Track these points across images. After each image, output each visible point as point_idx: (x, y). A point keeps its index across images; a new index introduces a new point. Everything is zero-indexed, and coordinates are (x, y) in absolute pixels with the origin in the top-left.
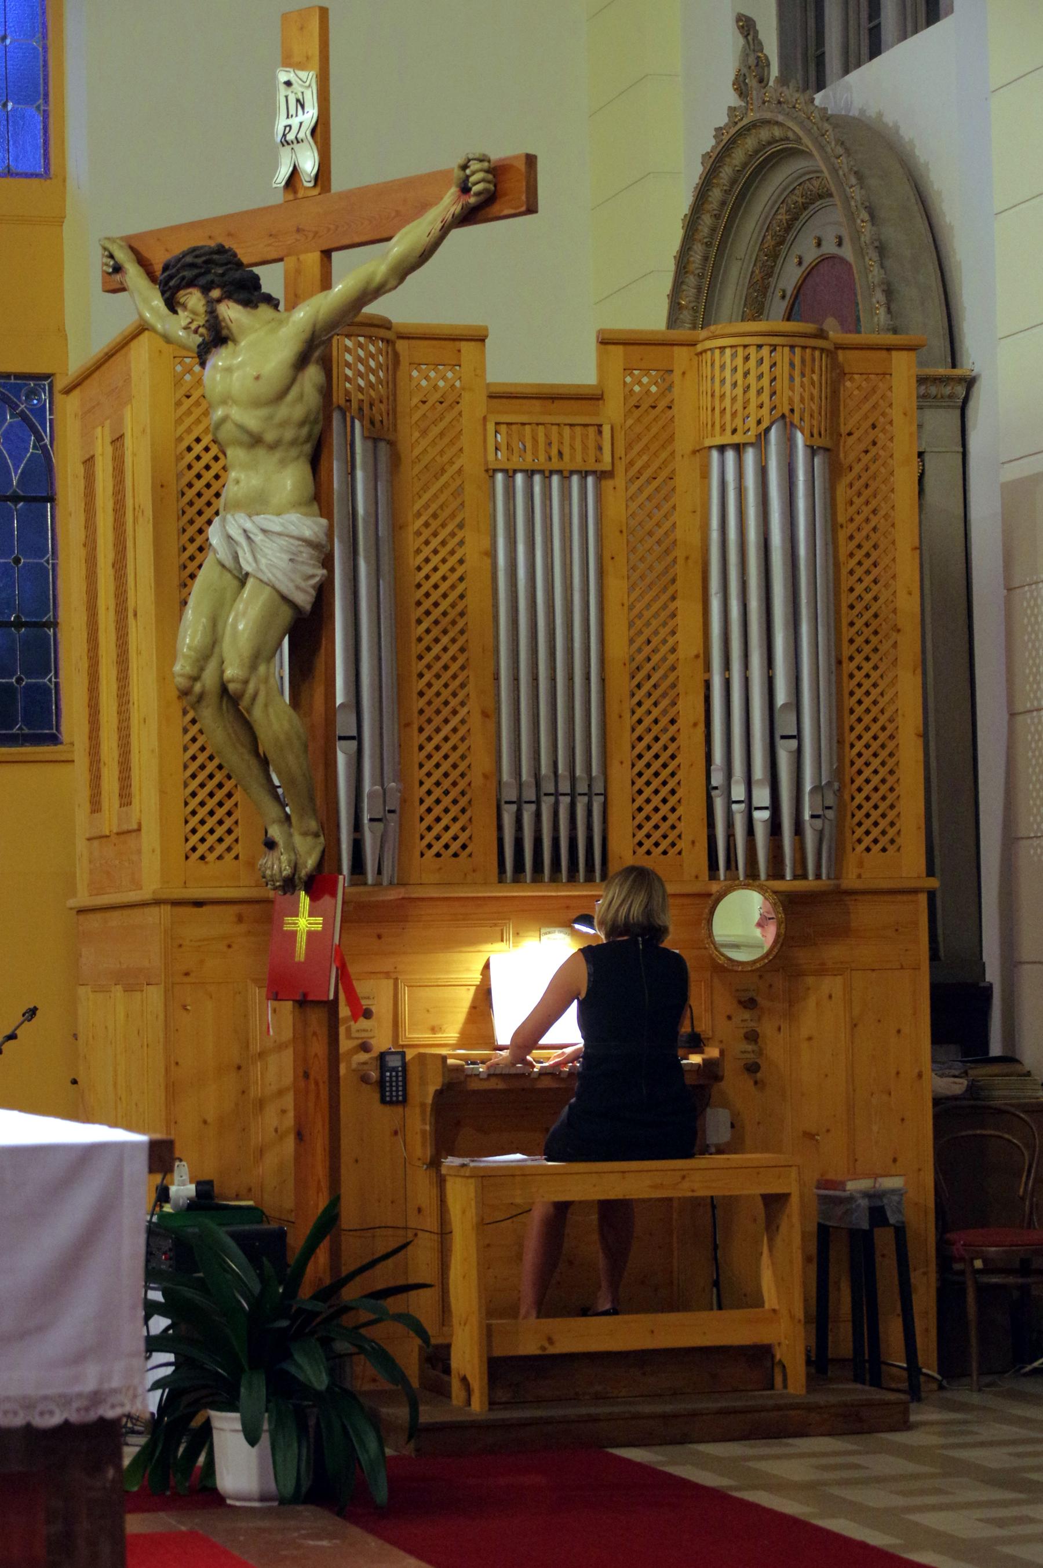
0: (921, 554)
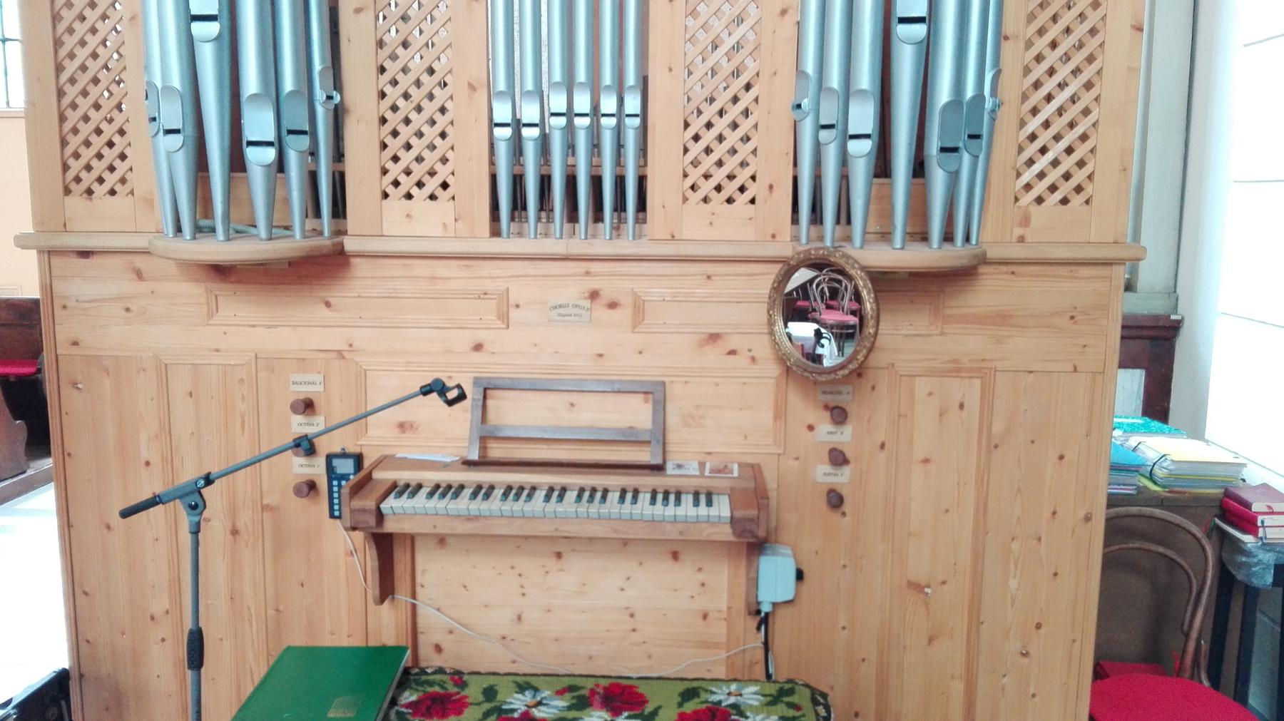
0: (978, 617)
